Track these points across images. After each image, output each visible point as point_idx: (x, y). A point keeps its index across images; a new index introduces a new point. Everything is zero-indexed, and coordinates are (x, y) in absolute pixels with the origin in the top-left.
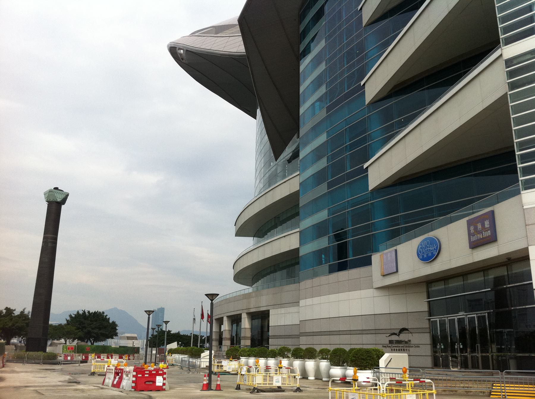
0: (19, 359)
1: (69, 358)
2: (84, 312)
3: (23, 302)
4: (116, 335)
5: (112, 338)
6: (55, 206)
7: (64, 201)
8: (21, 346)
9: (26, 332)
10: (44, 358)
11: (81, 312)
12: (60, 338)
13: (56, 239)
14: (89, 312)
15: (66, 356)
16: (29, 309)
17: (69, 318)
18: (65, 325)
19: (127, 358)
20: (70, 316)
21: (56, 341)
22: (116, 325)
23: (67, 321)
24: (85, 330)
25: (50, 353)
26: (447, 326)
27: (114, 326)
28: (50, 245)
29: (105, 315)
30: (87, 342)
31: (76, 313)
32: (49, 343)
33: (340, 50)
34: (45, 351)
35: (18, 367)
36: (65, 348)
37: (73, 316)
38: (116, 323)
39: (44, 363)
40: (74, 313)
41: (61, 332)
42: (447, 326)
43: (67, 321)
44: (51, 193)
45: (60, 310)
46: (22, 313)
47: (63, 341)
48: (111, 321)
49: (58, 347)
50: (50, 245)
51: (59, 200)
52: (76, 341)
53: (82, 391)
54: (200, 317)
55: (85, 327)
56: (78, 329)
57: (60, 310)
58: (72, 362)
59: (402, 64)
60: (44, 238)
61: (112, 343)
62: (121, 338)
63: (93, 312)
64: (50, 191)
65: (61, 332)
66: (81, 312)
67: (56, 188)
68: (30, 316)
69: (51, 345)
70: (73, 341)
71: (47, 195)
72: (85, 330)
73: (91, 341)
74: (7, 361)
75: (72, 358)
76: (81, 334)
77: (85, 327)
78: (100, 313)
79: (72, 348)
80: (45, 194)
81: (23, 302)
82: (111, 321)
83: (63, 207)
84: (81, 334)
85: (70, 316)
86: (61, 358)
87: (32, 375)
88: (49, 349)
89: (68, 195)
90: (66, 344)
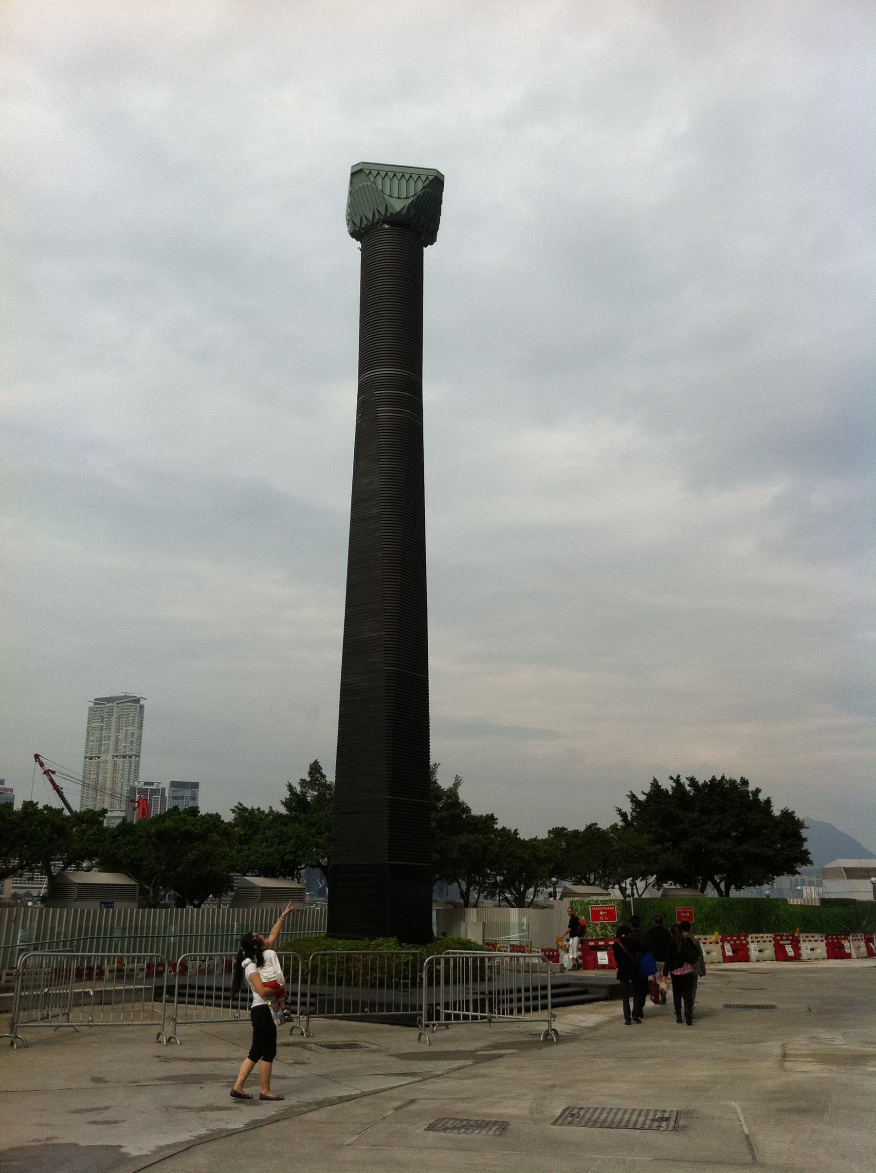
2: (677, 781)
4: (804, 858)
5: (794, 872)
9: (375, 868)
11: (718, 778)
14: (693, 782)
17: (628, 808)
19: (864, 949)
22: (799, 824)
26: (487, 1008)
27: (790, 827)
29: (751, 788)
30: (703, 890)
31: (648, 789)
37: (642, 798)
38: (799, 815)
42: (487, 1008)
48: (776, 812)
59: (444, 207)
61: (803, 890)
62: (827, 874)
63: (708, 779)
66: (667, 785)
73: (717, 886)
78: (732, 782)
82: (776, 812)
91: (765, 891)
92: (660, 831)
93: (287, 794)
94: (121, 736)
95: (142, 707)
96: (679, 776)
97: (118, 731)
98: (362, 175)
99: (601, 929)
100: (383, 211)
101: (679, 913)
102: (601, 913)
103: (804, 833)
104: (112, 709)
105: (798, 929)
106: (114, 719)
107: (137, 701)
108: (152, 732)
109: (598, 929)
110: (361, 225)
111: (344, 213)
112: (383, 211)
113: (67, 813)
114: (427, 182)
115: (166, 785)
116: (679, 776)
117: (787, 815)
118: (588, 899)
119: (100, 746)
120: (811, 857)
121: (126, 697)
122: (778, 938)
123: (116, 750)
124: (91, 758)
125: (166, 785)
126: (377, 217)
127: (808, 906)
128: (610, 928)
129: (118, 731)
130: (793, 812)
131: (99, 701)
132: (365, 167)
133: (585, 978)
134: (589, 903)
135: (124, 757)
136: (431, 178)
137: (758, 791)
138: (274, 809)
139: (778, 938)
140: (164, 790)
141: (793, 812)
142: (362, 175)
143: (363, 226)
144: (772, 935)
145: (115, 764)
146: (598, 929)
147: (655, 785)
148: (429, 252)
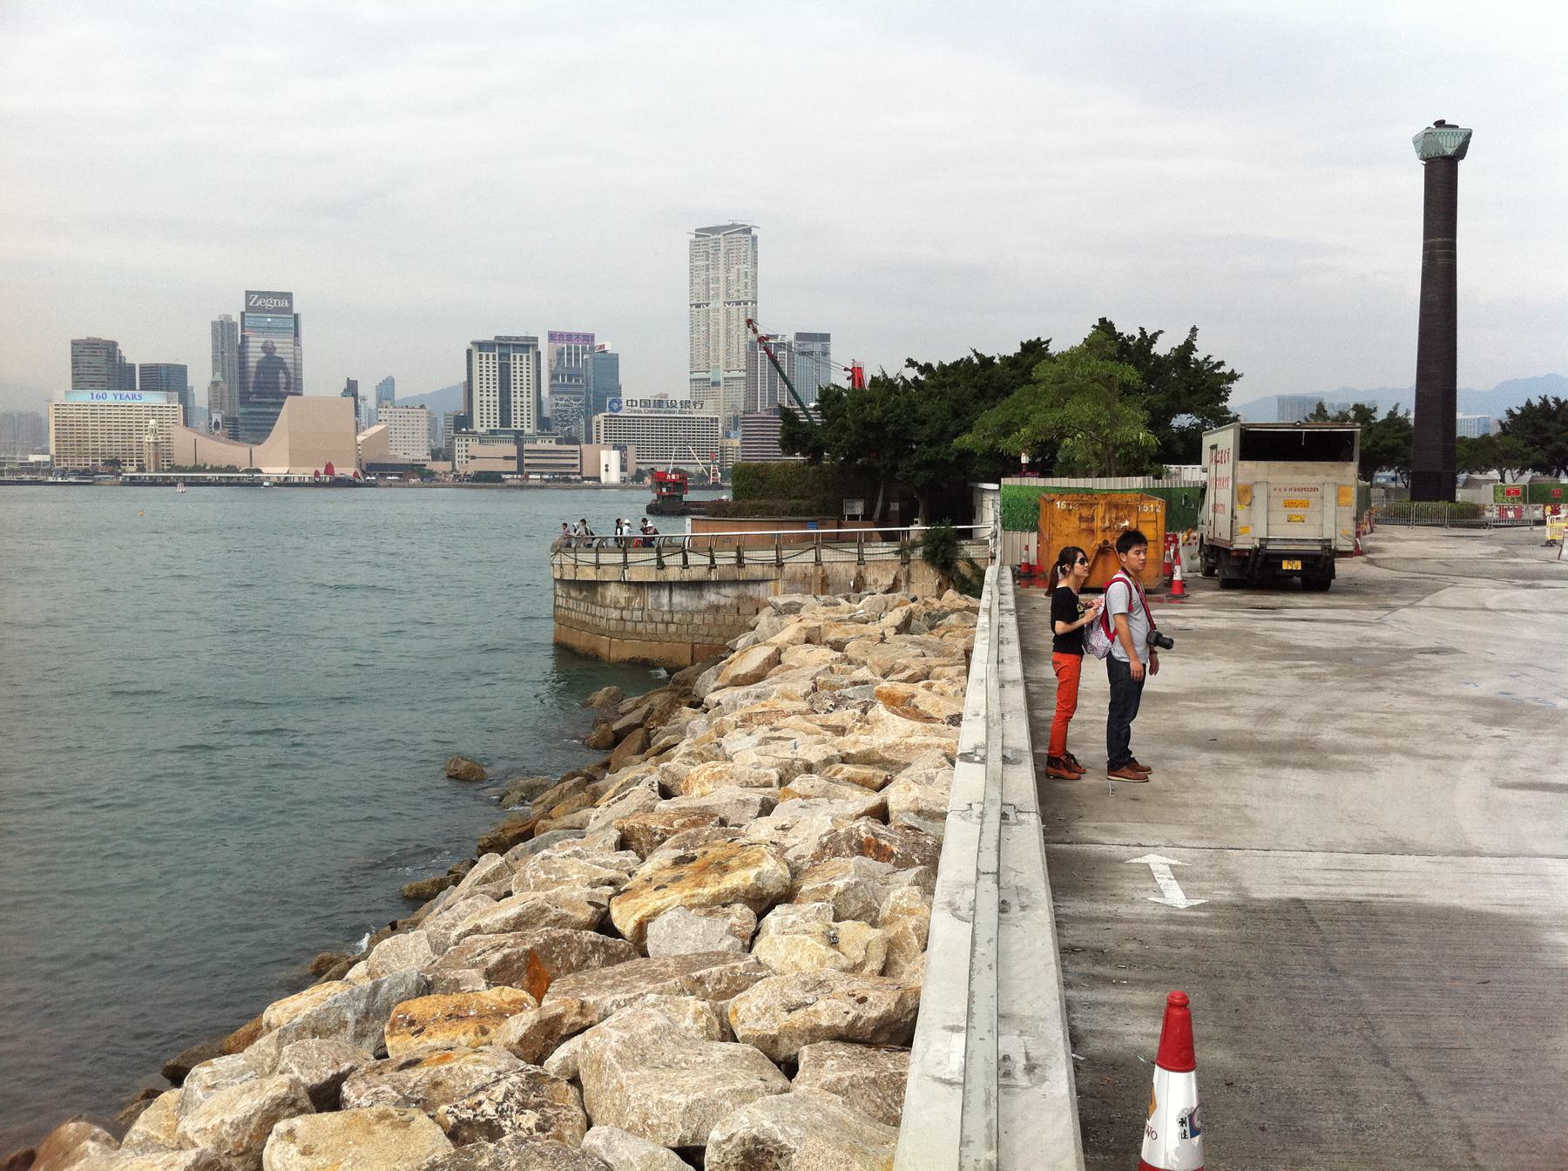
0: (1399, 517)
1: (1511, 514)
2: (1545, 401)
3: (1391, 384)
6: (1441, 174)
7: (1461, 152)
8: (1398, 489)
10: (1453, 515)
11: (1536, 402)
12: (1488, 468)
13: (1453, 246)
14: (1557, 400)
15: (1503, 511)
16: (1407, 408)
18: (1499, 436)
20: (1510, 413)
21: (1477, 476)
23: (1503, 426)
24: (1550, 447)
25: (1466, 504)
28: (1440, 261)
30: (1557, 476)
32: (1462, 477)
33: (1136, 889)
34: (1452, 499)
35: (1400, 531)
36: (1503, 493)
37: (1518, 412)
39: (1453, 526)
40: (1517, 406)
41: (1486, 453)
43: (1503, 426)
44: (1430, 138)
45: (1482, 402)
46: (1392, 414)
47: (1494, 474)
49: (1482, 489)
50: (1440, 261)
51: (1450, 151)
52: (1528, 475)
53: (1517, 564)
54: (975, 656)
55: (1549, 440)
56: (1532, 443)
57: (1482, 402)
58: (1519, 522)
60: (1426, 247)
64: (1428, 133)
65: (1486, 453)
66: (1536, 402)
67: (1440, 124)
68: (1412, 422)
69: (1467, 484)
70: (1521, 473)
71: (1420, 144)
72: (1550, 447)
74: (1377, 521)
75: (1518, 512)
76: (1538, 456)
77: (1549, 440)
79: (1517, 492)
80: (1415, 143)
81: (1391, 384)
83: (1461, 164)
84: (1538, 456)
85: (1510, 413)
86: (1491, 515)
87: (1434, 544)
88: (1461, 495)
89: (1470, 134)
90: (1502, 480)
93: (1215, 360)
94: (733, 276)
95: (755, 239)
97: (728, 271)
104: (717, 242)
106: (721, 255)
107: (748, 231)
108: (768, 267)
111: (97, 336)
113: (976, 361)
115: (790, 337)
119: (708, 290)
121: (733, 226)
123: (728, 295)
124: (698, 306)
125: (790, 337)
129: (728, 271)
131: (702, 233)
133: (761, 525)
135: (738, 303)
138: (1234, 386)
140: (790, 344)
145: (728, 313)
147: (1529, 403)
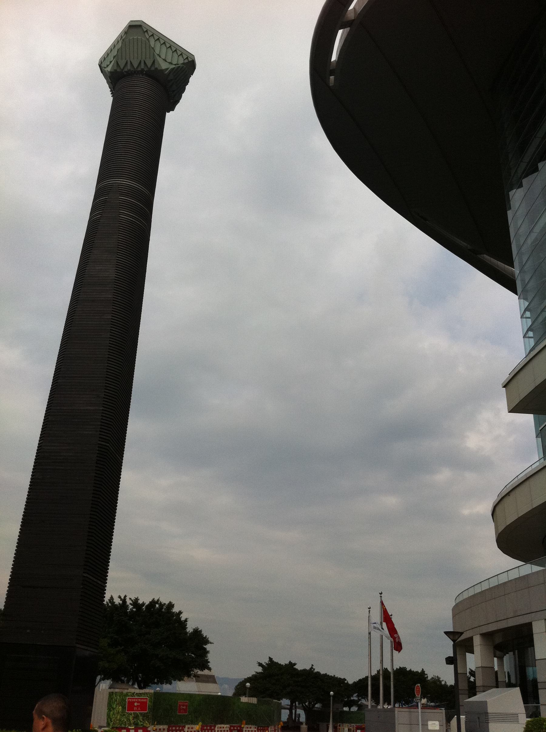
14: (135, 603)
27: (199, 641)
38: (205, 633)
48: (190, 629)
91: (166, 688)
92: (116, 637)
96: (125, 596)
98: (136, 30)
99: (134, 718)
100: (149, 64)
101: (180, 705)
102: (136, 704)
103: (208, 647)
105: (244, 722)
109: (131, 718)
110: (123, 69)
112: (149, 64)
114: (186, 61)
116: (125, 596)
117: (197, 632)
118: (126, 691)
120: (210, 665)
122: (232, 728)
126: (142, 66)
127: (250, 703)
128: (141, 718)
130: (201, 631)
132: (143, 24)
134: (127, 695)
136: (190, 60)
137: (180, 613)
139: (232, 728)
141: (201, 631)
142: (136, 30)
143: (126, 70)
144: (228, 726)
146: (131, 718)
148: (169, 116)
